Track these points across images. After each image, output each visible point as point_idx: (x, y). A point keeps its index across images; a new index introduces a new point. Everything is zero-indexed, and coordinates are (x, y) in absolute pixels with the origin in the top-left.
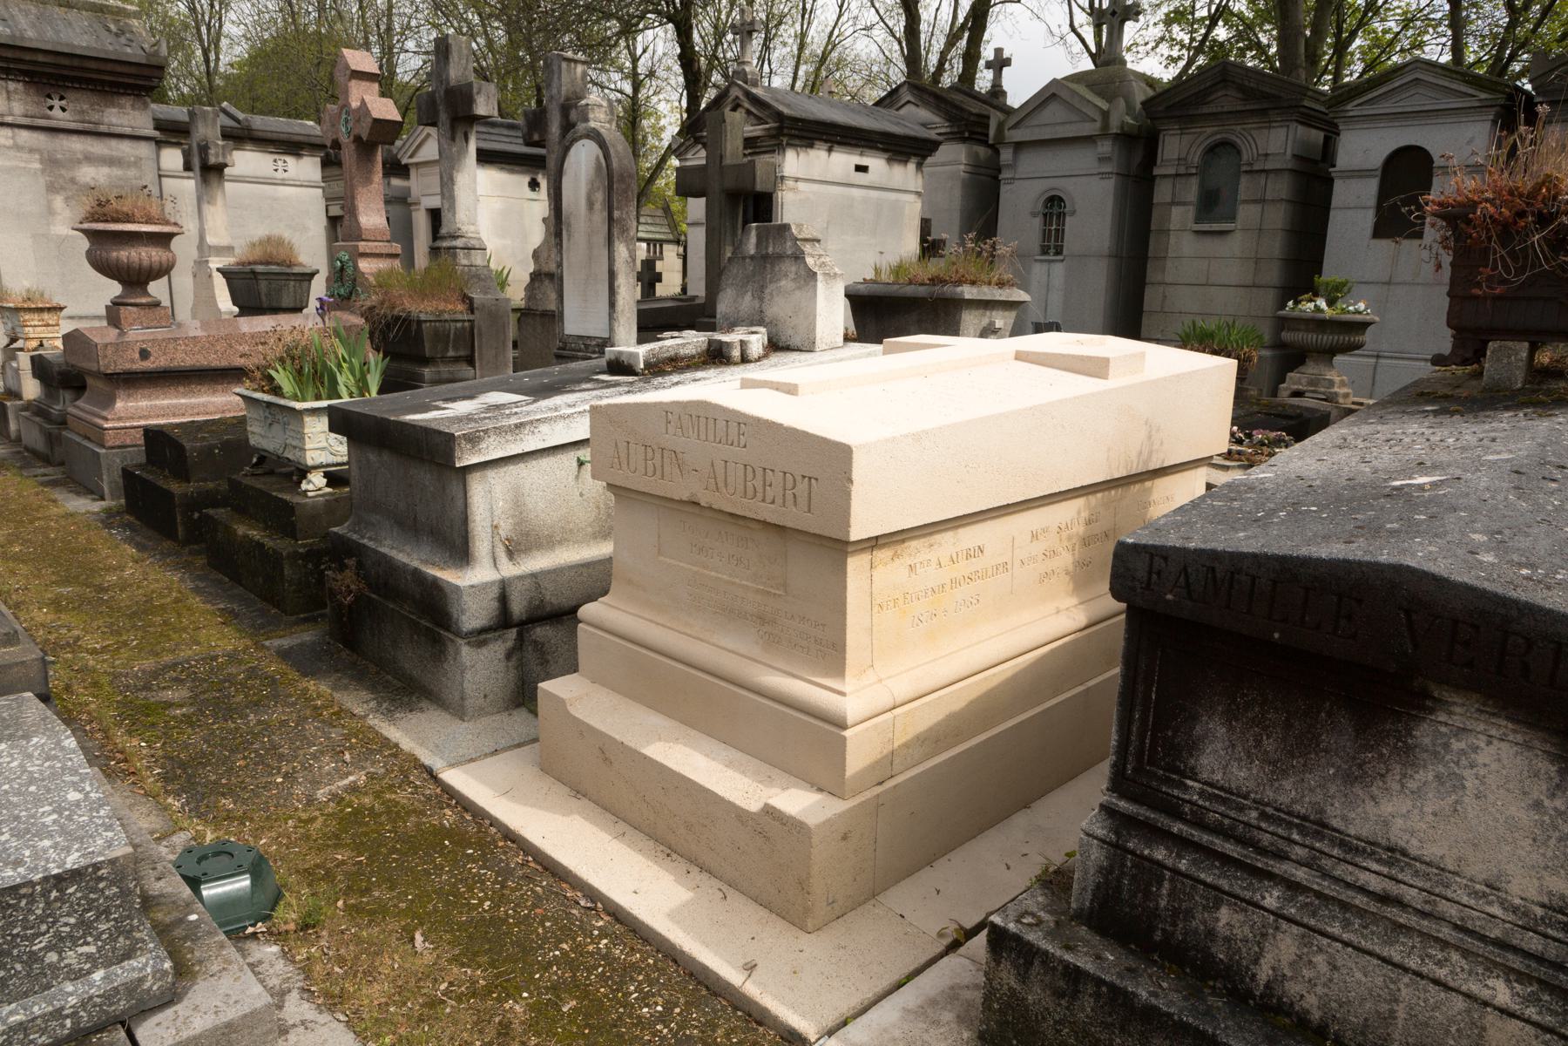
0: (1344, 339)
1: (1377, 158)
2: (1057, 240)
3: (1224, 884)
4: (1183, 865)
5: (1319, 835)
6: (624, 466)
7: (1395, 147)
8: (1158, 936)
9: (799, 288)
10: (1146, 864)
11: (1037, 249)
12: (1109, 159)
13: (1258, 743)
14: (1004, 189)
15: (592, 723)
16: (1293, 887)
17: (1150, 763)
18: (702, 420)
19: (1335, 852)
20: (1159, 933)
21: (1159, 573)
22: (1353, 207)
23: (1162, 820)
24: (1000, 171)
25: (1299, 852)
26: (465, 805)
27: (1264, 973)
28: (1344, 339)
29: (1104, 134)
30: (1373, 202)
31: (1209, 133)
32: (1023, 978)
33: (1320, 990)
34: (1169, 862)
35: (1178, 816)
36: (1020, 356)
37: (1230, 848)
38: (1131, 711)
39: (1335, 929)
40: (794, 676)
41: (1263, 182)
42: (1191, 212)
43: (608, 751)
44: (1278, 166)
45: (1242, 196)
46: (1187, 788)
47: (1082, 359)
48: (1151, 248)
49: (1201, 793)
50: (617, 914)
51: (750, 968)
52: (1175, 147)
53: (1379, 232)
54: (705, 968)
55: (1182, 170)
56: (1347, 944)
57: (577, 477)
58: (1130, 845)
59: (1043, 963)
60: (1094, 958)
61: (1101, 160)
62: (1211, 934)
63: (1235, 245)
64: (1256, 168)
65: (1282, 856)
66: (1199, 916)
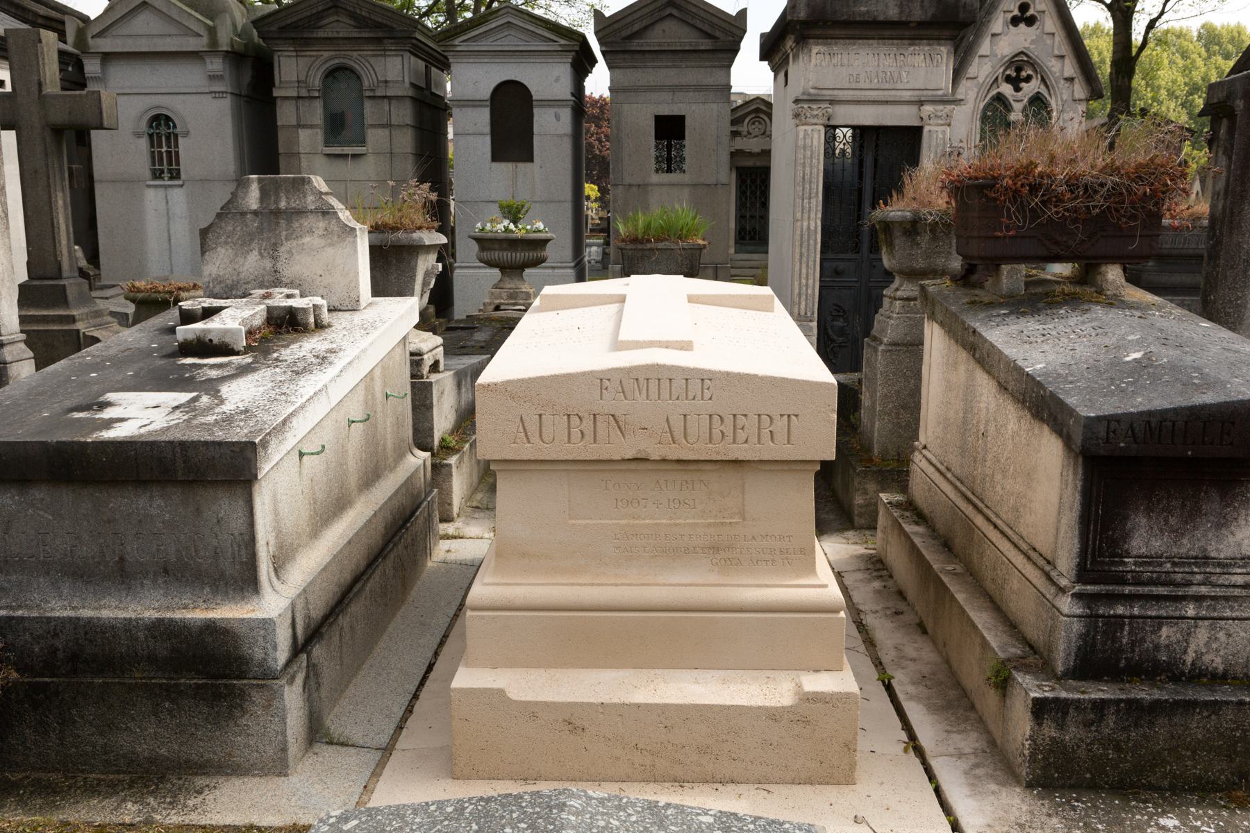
0: (533, 255)
2: (170, 163)
3: (1163, 613)
4: (1136, 611)
5: (1206, 564)
6: (535, 438)
7: (493, 86)
8: (1123, 663)
9: (332, 245)
11: (148, 174)
12: (221, 78)
13: (1166, 522)
15: (549, 699)
16: (1198, 599)
18: (653, 385)
19: (1218, 570)
22: (467, 137)
23: (1117, 589)
25: (1199, 577)
27: (1190, 657)
28: (533, 255)
29: (213, 50)
30: (487, 129)
31: (326, 58)
32: (1061, 726)
33: (1222, 653)
34: (1128, 613)
35: (1124, 582)
36: (692, 299)
37: (1162, 590)
38: (1088, 526)
39: (1228, 613)
40: (767, 586)
41: (387, 108)
42: (319, 135)
43: (573, 719)
44: (400, 94)
45: (369, 120)
46: (1125, 563)
49: (1135, 564)
52: (291, 70)
53: (497, 156)
55: (304, 93)
56: (1234, 619)
58: (1101, 612)
62: (1157, 647)
64: (378, 94)
65: (1189, 584)
66: (1148, 639)
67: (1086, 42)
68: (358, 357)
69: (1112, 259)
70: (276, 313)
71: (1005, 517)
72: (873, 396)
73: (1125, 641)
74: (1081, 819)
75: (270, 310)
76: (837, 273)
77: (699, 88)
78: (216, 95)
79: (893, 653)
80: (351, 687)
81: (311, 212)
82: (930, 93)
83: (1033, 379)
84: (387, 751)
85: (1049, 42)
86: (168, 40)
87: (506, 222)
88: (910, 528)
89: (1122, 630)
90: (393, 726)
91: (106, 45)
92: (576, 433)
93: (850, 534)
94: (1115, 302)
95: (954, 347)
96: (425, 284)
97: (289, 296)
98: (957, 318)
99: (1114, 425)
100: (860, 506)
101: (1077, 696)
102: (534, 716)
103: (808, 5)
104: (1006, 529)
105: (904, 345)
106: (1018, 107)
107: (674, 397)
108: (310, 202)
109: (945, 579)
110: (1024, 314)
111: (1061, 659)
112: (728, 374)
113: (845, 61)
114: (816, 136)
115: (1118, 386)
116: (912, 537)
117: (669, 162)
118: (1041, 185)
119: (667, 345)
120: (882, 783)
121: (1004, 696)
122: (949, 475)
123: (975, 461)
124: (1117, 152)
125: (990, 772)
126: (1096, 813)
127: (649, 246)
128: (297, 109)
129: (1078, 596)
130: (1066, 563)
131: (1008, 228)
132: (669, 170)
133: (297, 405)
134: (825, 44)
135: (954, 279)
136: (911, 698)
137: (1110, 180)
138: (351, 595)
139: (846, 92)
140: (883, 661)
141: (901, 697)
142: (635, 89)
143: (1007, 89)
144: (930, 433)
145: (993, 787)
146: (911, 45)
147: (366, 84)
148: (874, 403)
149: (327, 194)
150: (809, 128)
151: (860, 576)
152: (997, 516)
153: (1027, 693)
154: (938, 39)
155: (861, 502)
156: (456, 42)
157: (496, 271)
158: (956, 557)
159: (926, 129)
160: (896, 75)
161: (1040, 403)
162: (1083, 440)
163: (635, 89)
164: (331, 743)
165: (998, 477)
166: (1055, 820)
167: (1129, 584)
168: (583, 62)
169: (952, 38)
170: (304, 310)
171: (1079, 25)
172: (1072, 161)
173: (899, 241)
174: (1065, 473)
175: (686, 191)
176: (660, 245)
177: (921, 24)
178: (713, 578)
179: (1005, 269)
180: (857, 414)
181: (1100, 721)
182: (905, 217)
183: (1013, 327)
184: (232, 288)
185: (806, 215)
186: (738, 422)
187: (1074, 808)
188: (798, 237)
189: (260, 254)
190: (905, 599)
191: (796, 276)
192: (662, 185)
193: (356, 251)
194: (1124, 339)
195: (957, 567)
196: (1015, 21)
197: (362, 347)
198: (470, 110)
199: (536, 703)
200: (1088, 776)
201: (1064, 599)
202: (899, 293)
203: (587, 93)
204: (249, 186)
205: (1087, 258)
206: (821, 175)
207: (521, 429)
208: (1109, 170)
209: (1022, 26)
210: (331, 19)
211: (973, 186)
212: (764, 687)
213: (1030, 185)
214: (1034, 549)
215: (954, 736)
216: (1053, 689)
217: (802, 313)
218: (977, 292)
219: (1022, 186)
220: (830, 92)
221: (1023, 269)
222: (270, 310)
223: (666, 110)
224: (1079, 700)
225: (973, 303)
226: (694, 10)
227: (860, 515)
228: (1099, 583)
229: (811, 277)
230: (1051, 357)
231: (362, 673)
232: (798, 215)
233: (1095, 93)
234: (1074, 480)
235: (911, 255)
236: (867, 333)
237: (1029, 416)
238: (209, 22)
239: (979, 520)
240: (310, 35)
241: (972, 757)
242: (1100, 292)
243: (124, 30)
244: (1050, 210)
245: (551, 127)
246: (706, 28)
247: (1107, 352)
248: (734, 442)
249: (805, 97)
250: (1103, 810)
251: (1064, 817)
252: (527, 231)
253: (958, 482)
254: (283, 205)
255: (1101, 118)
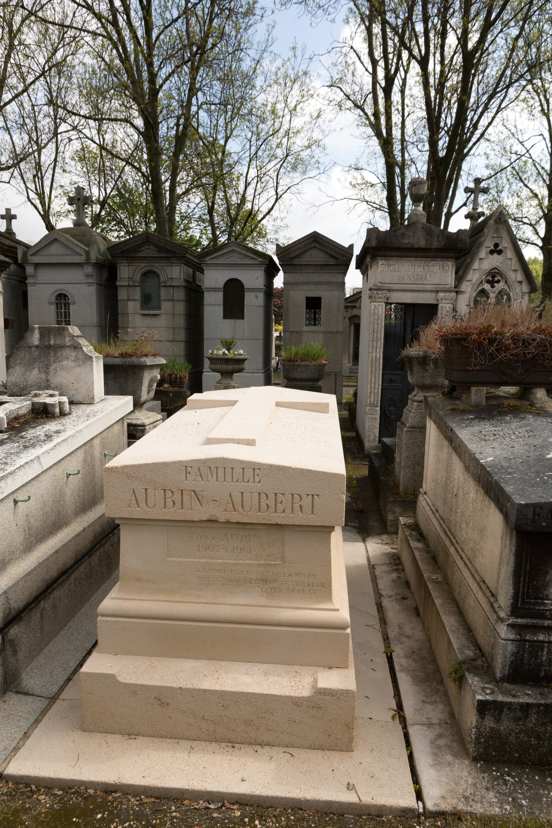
0: (237, 367)
1: (221, 284)
2: (65, 317)
6: (143, 504)
7: (225, 281)
9: (79, 366)
10: (536, 644)
14: (30, 289)
17: (527, 598)
18: (221, 471)
20: (543, 672)
21: (538, 515)
22: (213, 305)
23: (540, 622)
24: (26, 279)
26: (47, 785)
28: (237, 367)
29: (88, 262)
30: (221, 302)
31: (143, 267)
32: (498, 720)
34: (546, 640)
35: (544, 618)
41: (172, 291)
42: (138, 304)
43: (161, 697)
45: (162, 298)
46: (545, 604)
47: (314, 404)
48: (119, 322)
50: (241, 801)
51: (350, 787)
52: (126, 272)
54: (329, 804)
55: (131, 284)
57: (14, 513)
58: (527, 638)
59: (509, 709)
60: (526, 696)
61: (87, 276)
63: (163, 321)
64: (168, 284)
67: (530, 266)
68: (73, 436)
69: (540, 385)
70: (37, 406)
71: (467, 553)
72: (400, 456)
73: (544, 659)
74: (510, 794)
75: (33, 404)
76: (391, 381)
77: (329, 283)
78: (89, 284)
79: (396, 630)
80: (50, 646)
81: (68, 347)
82: (442, 286)
83: (485, 469)
84: (53, 699)
85: (509, 263)
86: (66, 257)
87: (224, 350)
88: (415, 544)
89: (543, 650)
90: (65, 678)
91: (36, 259)
92: (169, 501)
93: (385, 537)
94: (541, 412)
95: (442, 437)
96: (150, 386)
97: (51, 396)
98: (443, 419)
99: (538, 510)
100: (391, 521)
101: (510, 700)
102: (135, 693)
103: (377, 239)
104: (467, 562)
105: (419, 428)
106: (492, 295)
107: (235, 480)
108: (68, 341)
109: (430, 586)
110: (483, 419)
111: (500, 666)
112: (271, 466)
113: (397, 269)
114: (380, 308)
115: (542, 478)
116: (414, 551)
117: (314, 320)
118: (496, 339)
119: (238, 442)
120: (372, 751)
121: (460, 687)
122: (437, 515)
123: (451, 511)
124: (543, 320)
125: (449, 743)
126: (521, 788)
127: (297, 363)
128: (128, 291)
129: (512, 626)
130: (505, 598)
131: (475, 365)
132: (315, 325)
133: (6, 472)
134: (385, 260)
135: (443, 394)
136: (403, 670)
137: (539, 337)
138: (55, 585)
139: (397, 285)
140: (390, 636)
141: (397, 668)
142: (296, 284)
143: (487, 287)
144: (428, 486)
145: (449, 758)
146: (432, 261)
147: (162, 279)
148: (401, 460)
149: (78, 336)
150: (377, 304)
151: (385, 568)
152: (463, 551)
153: (474, 695)
154: (447, 258)
155: (391, 518)
156: (207, 259)
157: (218, 374)
158: (439, 568)
159: (440, 305)
160: (424, 277)
161: (490, 486)
162: (516, 520)
163: (296, 284)
164: (17, 692)
165: (464, 526)
166: (491, 794)
167: (548, 619)
168: (271, 271)
169: (457, 259)
170: (53, 405)
171: (526, 258)
172: (515, 326)
173: (416, 368)
174: (504, 538)
175: (321, 336)
176: (303, 363)
177: (437, 250)
178: (263, 601)
179: (474, 389)
180: (392, 465)
181: (526, 719)
182: (419, 355)
183: (476, 428)
184: (23, 389)
185: (374, 350)
186: (278, 498)
187: (506, 783)
188: (370, 362)
189: (39, 370)
190: (409, 587)
191: (369, 383)
192: (309, 332)
193: (92, 370)
194: (547, 441)
195: (439, 576)
196: (492, 252)
197: (78, 429)
198: (213, 293)
199: (136, 685)
200: (517, 755)
201: (502, 626)
202: (416, 398)
203: (275, 287)
204: (34, 331)
205: (524, 384)
206: (383, 329)
207: (133, 498)
208: (538, 331)
209: (495, 255)
210: (146, 247)
211: (456, 339)
212: (292, 680)
213: (489, 339)
214: (484, 582)
215: (427, 706)
216: (493, 693)
217: (372, 402)
218: (457, 402)
219: (484, 339)
220: (388, 285)
221: (484, 389)
222: (33, 404)
223: (311, 294)
224: (511, 703)
225: (453, 410)
226: (326, 244)
227: (391, 526)
228: (526, 617)
229: (377, 383)
230: (498, 452)
231: (62, 633)
232: (371, 350)
233: (533, 289)
234: (510, 544)
235: (423, 376)
236: (399, 420)
237: (482, 492)
238: (87, 249)
239: (452, 550)
240: (133, 255)
241: (437, 727)
242: (532, 405)
243: (45, 252)
244: (501, 354)
245: (254, 302)
246: (334, 254)
247: (535, 450)
248: (276, 512)
249: (375, 288)
250: (527, 785)
251: (498, 792)
252: (235, 355)
253: (442, 519)
254: (52, 342)
255: (537, 302)
